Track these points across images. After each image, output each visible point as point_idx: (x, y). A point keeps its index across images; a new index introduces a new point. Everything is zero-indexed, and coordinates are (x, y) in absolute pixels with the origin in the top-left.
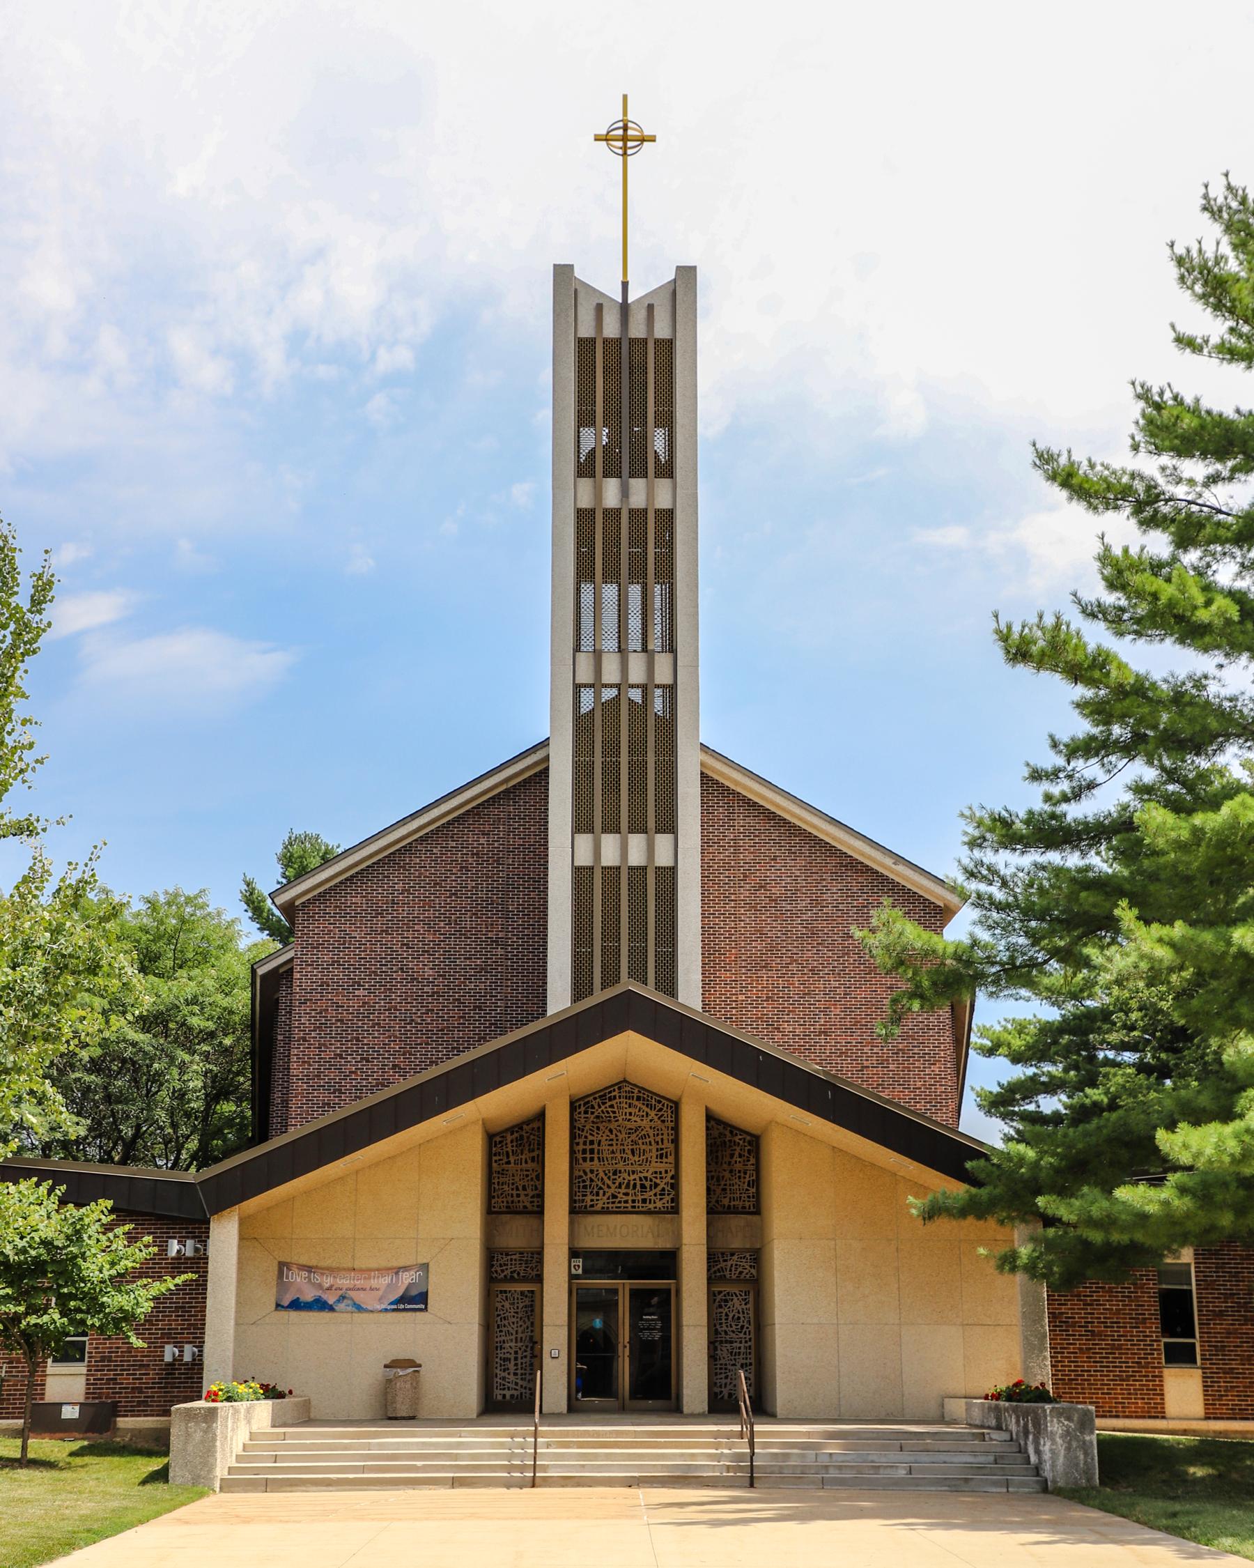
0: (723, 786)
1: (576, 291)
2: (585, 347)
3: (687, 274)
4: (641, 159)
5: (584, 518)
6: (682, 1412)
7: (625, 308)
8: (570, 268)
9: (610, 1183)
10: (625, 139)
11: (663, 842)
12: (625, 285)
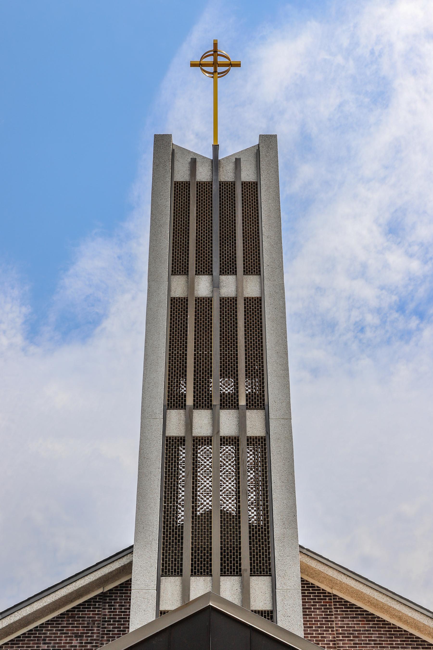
0: (319, 589)
1: (173, 150)
2: (180, 190)
3: (269, 141)
4: (229, 83)
5: (177, 306)
6: (272, 612)
7: (215, 164)
8: (168, 137)
9: (203, 486)
10: (215, 64)
11: (259, 586)
12: (216, 148)
